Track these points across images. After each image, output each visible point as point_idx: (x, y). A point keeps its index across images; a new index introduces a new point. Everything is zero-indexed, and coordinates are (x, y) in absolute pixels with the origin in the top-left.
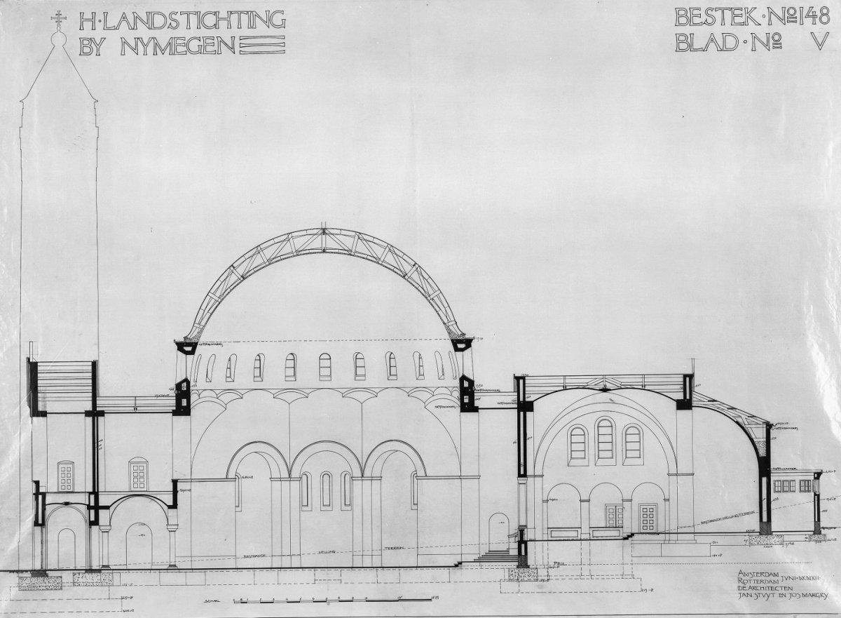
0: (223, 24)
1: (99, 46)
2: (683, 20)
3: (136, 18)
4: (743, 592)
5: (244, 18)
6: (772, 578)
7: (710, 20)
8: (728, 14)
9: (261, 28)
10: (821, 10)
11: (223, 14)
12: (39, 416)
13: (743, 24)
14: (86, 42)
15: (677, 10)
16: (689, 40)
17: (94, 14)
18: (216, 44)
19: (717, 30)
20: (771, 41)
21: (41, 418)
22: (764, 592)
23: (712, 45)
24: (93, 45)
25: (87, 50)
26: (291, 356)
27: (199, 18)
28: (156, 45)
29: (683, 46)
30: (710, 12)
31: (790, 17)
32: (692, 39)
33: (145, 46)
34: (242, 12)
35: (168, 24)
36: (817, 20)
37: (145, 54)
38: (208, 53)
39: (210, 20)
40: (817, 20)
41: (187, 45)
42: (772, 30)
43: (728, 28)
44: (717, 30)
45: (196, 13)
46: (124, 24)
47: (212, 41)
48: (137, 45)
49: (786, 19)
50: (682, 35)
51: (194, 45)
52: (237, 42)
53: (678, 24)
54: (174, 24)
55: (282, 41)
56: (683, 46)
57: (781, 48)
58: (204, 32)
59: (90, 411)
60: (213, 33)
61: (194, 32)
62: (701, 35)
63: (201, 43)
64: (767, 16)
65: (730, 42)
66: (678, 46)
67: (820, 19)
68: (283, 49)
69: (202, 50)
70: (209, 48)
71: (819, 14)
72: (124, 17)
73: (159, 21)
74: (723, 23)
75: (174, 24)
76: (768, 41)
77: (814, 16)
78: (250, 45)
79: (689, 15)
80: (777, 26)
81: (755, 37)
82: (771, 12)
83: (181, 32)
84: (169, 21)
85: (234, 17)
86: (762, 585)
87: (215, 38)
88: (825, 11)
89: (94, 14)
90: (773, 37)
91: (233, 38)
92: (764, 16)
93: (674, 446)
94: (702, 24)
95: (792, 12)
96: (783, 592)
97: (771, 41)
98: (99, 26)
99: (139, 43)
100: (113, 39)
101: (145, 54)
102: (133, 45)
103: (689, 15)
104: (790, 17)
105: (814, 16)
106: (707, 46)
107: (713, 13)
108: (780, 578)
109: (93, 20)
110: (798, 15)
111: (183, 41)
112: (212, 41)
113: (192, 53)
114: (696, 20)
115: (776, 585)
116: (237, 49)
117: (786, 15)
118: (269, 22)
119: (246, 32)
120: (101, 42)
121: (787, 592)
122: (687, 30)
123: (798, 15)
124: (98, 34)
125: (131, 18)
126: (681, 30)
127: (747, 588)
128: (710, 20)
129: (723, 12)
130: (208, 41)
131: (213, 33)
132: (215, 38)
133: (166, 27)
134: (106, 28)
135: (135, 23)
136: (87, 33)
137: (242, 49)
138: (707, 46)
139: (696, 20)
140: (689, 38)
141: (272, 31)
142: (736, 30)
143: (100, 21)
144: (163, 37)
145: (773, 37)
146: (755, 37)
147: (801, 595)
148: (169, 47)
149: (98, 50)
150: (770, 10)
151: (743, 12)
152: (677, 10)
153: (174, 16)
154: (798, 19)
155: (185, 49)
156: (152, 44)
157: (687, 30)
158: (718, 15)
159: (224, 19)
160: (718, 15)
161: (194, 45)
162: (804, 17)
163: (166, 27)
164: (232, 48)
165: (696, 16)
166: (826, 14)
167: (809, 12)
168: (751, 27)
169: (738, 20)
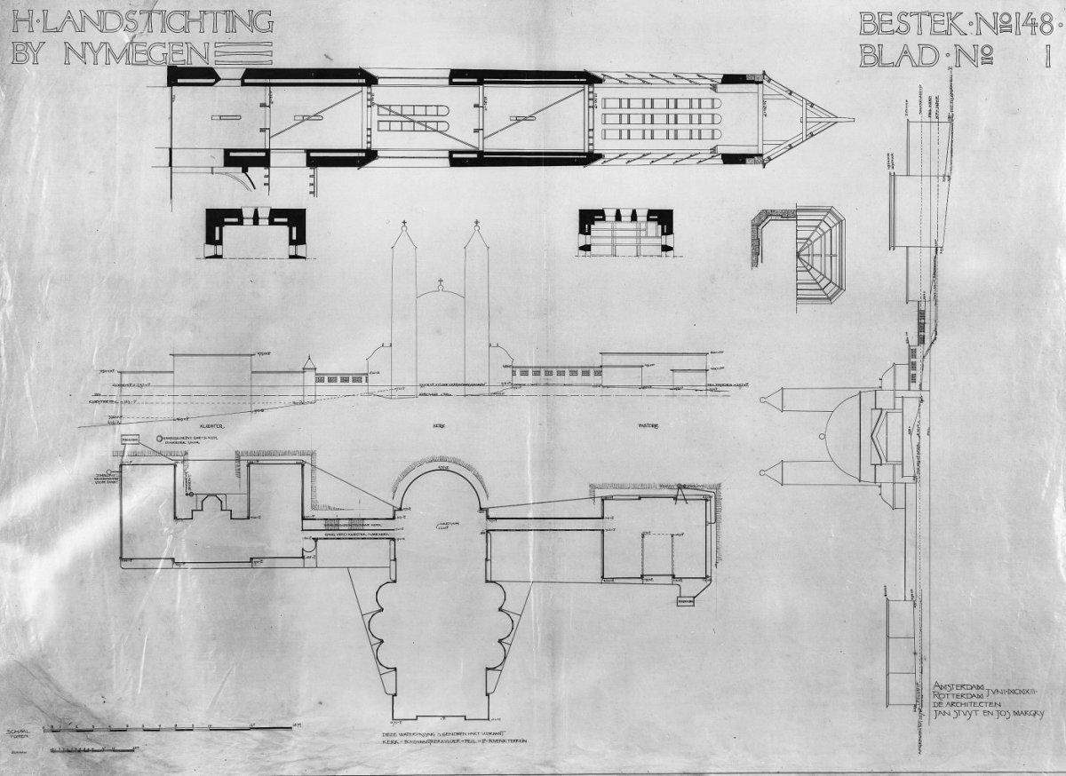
0: (194, 27)
1: (37, 51)
2: (870, 28)
3: (85, 17)
4: (938, 709)
6: (974, 691)
7: (903, 28)
8: (926, 20)
9: (243, 33)
10: (1042, 18)
14: (20, 48)
16: (877, 53)
18: (185, 52)
22: (963, 708)
24: (29, 51)
26: (931, 60)
27: (163, 17)
30: (903, 18)
31: (1003, 25)
32: (881, 53)
33: (95, 53)
34: (922, 13)
36: (1037, 29)
37: (96, 63)
39: (178, 21)
40: (1037, 29)
41: (148, 53)
42: (981, 42)
43: (926, 38)
44: (912, 40)
46: (69, 24)
49: (999, 29)
50: (866, 46)
52: (212, 49)
55: (268, 48)
56: (870, 60)
57: (992, 63)
60: (182, 37)
61: (157, 36)
63: (166, 50)
64: (975, 23)
66: (863, 59)
67: (1041, 30)
68: (270, 58)
71: (1039, 22)
72: (69, 17)
73: (112, 21)
77: (1034, 25)
79: (877, 21)
80: (988, 36)
81: (960, 50)
82: (980, 17)
84: (126, 22)
85: (209, 19)
86: (963, 700)
88: (1047, 18)
90: (982, 51)
92: (971, 24)
93: (873, 446)
95: (1006, 18)
97: (980, 55)
98: (38, 27)
101: (96, 63)
103: (877, 21)
104: (1003, 25)
106: (900, 59)
107: (907, 19)
108: (985, 693)
109: (29, 20)
110: (1013, 22)
114: (886, 27)
115: (980, 700)
117: (999, 23)
118: (252, 25)
119: (222, 36)
120: (39, 48)
122: (874, 40)
123: (1013, 22)
124: (35, 39)
127: (944, 705)
128: (903, 28)
131: (182, 37)
134: (45, 30)
135: (83, 23)
137: (217, 59)
138: (900, 59)
139: (886, 27)
140: (877, 49)
141: (255, 36)
143: (38, 21)
145: (982, 51)
147: (1012, 713)
149: (35, 57)
150: (979, 16)
153: (131, 16)
157: (874, 40)
159: (194, 20)
160: (913, 21)
165: (886, 22)
166: (1049, 23)
167: (1027, 19)
168: (955, 37)
169: (938, 28)
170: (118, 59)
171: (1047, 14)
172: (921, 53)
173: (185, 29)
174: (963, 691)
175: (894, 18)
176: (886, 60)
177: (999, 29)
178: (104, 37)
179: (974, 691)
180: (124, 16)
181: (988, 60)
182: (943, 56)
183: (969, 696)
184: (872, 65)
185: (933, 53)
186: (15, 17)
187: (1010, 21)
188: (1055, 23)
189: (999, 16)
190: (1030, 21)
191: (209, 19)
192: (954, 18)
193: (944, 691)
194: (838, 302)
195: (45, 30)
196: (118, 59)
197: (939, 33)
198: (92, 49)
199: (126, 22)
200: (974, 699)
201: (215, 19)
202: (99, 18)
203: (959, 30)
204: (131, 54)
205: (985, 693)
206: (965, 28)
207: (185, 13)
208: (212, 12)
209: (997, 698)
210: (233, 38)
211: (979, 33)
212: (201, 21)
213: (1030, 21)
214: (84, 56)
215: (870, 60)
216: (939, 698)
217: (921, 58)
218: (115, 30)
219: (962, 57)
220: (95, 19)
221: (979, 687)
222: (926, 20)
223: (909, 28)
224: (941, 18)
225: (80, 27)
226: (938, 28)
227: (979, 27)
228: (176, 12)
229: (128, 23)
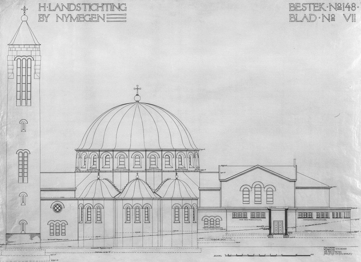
0: (100, 9)
2: (292, 9)
3: (63, 5)
7: (304, 8)
8: (312, 6)
9: (116, 11)
10: (352, 5)
13: (319, 10)
16: (295, 17)
19: (307, 12)
20: (331, 18)
24: (44, 17)
29: (293, 19)
30: (304, 5)
31: (338, 7)
35: (76, 9)
37: (67, 21)
38: (94, 21)
39: (95, 7)
40: (350, 9)
42: (331, 13)
43: (312, 12)
44: (307, 12)
45: (88, 4)
47: (95, 16)
48: (75, 19)
49: (337, 9)
52: (106, 16)
53: (40, 10)
54: (79, 9)
55: (125, 16)
56: (293, 19)
58: (92, 12)
60: (96, 13)
61: (88, 12)
62: (300, 15)
63: (90, 17)
65: (313, 18)
66: (290, 19)
70: (94, 19)
72: (58, 6)
73: (72, 7)
74: (107, 10)
75: (79, 9)
76: (329, 18)
77: (349, 7)
80: (333, 11)
81: (324, 16)
82: (331, 5)
84: (77, 8)
86: (331, 249)
87: (97, 15)
88: (354, 5)
89: (45, 4)
92: (327, 7)
94: (301, 10)
95: (339, 5)
99: (64, 16)
100: (53, 15)
101: (67, 21)
103: (295, 6)
105: (349, 7)
106: (303, 19)
107: (306, 6)
108: (335, 249)
110: (342, 6)
111: (83, 16)
112: (95, 16)
113: (87, 21)
114: (298, 8)
116: (106, 20)
117: (337, 7)
119: (110, 12)
120: (48, 17)
122: (294, 13)
123: (342, 6)
126: (292, 12)
128: (304, 8)
130: (93, 16)
131: (96, 13)
132: (97, 15)
133: (76, 10)
134: (50, 10)
136: (42, 12)
140: (295, 16)
143: (47, 7)
146: (324, 16)
151: (318, 5)
154: (342, 9)
155: (83, 19)
158: (308, 6)
161: (87, 18)
162: (345, 7)
163: (76, 10)
164: (103, 20)
165: (94, 18)
169: (316, 8)
171: (353, 3)
172: (310, 17)
175: (301, 5)
177: (337, 9)
181: (333, 19)
182: (318, 18)
185: (73, 9)
186: (40, 6)
188: (356, 7)
190: (348, 6)
191: (105, 7)
194: (52, 209)
196: (74, 20)
198: (65, 17)
199: (77, 8)
201: (107, 7)
202: (68, 7)
203: (323, 9)
204: (78, 18)
206: (325, 8)
207: (96, 4)
208: (106, 4)
213: (348, 6)
217: (310, 17)
220: (115, 8)
222: (109, 6)
223: (80, 9)
225: (61, 9)
227: (330, 8)
228: (94, 4)
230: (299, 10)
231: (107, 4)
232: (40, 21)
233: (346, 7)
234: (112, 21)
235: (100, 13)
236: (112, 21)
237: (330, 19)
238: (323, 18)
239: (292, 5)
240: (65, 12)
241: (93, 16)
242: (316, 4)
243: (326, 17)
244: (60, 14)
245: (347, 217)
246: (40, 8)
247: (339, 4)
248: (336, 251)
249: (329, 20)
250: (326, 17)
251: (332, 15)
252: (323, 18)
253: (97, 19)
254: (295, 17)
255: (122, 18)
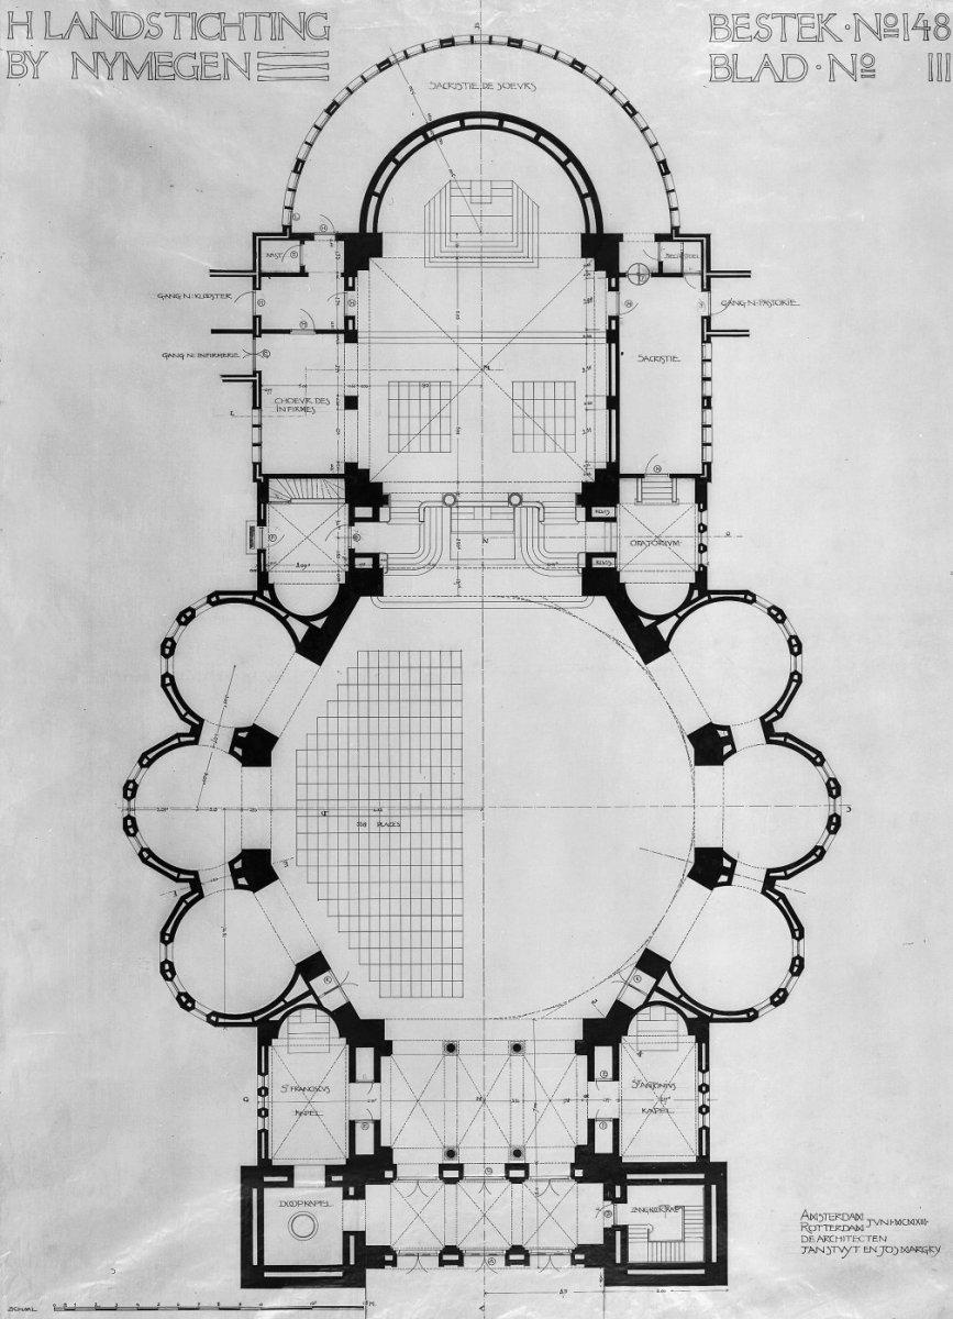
0: (232, 33)
3: (96, 20)
5: (266, 23)
9: (292, 41)
11: (232, 17)
12: (242, 1194)
13: (817, 39)
15: (713, 17)
16: (731, 63)
17: (29, 14)
18: (221, 64)
19: (775, 49)
20: (859, 67)
21: (239, 1199)
23: (767, 74)
25: (17, 70)
28: (127, 62)
30: (763, 21)
35: (145, 32)
38: (209, 79)
39: (211, 26)
40: (931, 33)
43: (793, 46)
46: (77, 29)
48: (96, 63)
51: (186, 66)
52: (254, 61)
55: (935, 57)
56: (721, 73)
58: (201, 45)
59: (372, 1183)
60: (217, 46)
61: (186, 44)
63: (198, 62)
65: (795, 68)
69: (198, 75)
71: (932, 25)
72: (76, 20)
74: (258, 37)
75: (154, 31)
76: (854, 68)
77: (926, 29)
78: (276, 67)
80: (870, 44)
81: (833, 61)
83: (165, 44)
84: (147, 27)
85: (249, 23)
86: (839, 1234)
89: (29, 14)
91: (247, 55)
92: (847, 27)
94: (751, 38)
95: (891, 20)
96: (874, 1245)
97: (859, 67)
99: (100, 60)
101: (110, 78)
102: (91, 64)
104: (885, 28)
105: (926, 29)
106: (759, 72)
107: (769, 22)
109: (28, 24)
110: (900, 26)
113: (183, 77)
114: (742, 32)
116: (254, 73)
117: (883, 26)
118: (304, 29)
119: (267, 45)
121: (877, 1244)
123: (900, 26)
124: (36, 46)
125: (87, 21)
127: (816, 1238)
128: (763, 33)
129: (177, 21)
131: (217, 46)
134: (48, 35)
136: (21, 42)
140: (731, 59)
141: (310, 45)
142: (805, 49)
144: (138, 52)
146: (833, 61)
148: (129, 68)
149: (36, 70)
151: (816, 21)
152: (713, 17)
153: (154, 19)
156: (119, 64)
157: (728, 47)
158: (776, 24)
159: (18, 24)
162: (910, 27)
165: (209, 64)
166: (944, 25)
169: (808, 33)
170: (138, 74)
173: (221, 36)
174: (839, 1222)
176: (742, 72)
178: (121, 46)
179: (852, 1222)
180: (145, 18)
182: (812, 65)
183: (846, 1228)
184: (724, 80)
186: (10, 19)
187: (896, 24)
189: (883, 17)
191: (249, 23)
192: (827, 20)
193: (813, 1222)
195: (48, 35)
196: (138, 74)
197: (808, 40)
200: (852, 1232)
201: (257, 22)
203: (833, 35)
205: (866, 1223)
209: (883, 1230)
210: (277, 47)
211: (858, 39)
212: (239, 25)
213: (921, 24)
214: (247, 71)
215: (721, 73)
216: (810, 1231)
218: (135, 36)
219: (837, 68)
221: (857, 1217)
222: (792, 25)
223: (161, 30)
224: (809, 20)
226: (808, 33)
229: (149, 27)
230: (742, 40)
231: (258, 16)
232: (11, 75)
233: (915, 28)
234: (301, 79)
235: (233, 47)
236: (301, 79)
237: (859, 73)
238: (832, 68)
239: (719, 21)
240: (110, 46)
241: (209, 59)
242: (805, 15)
243: (841, 66)
244: (86, 50)
245: (664, 1244)
246: (11, 28)
247: (888, 15)
248: (867, 1231)
249: (852, 74)
250: (841, 66)
251: (864, 57)
252: (832, 68)
253: (220, 70)
254: (731, 63)
255: (281, 67)
